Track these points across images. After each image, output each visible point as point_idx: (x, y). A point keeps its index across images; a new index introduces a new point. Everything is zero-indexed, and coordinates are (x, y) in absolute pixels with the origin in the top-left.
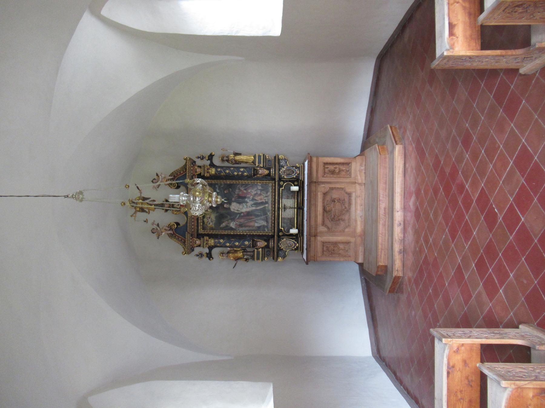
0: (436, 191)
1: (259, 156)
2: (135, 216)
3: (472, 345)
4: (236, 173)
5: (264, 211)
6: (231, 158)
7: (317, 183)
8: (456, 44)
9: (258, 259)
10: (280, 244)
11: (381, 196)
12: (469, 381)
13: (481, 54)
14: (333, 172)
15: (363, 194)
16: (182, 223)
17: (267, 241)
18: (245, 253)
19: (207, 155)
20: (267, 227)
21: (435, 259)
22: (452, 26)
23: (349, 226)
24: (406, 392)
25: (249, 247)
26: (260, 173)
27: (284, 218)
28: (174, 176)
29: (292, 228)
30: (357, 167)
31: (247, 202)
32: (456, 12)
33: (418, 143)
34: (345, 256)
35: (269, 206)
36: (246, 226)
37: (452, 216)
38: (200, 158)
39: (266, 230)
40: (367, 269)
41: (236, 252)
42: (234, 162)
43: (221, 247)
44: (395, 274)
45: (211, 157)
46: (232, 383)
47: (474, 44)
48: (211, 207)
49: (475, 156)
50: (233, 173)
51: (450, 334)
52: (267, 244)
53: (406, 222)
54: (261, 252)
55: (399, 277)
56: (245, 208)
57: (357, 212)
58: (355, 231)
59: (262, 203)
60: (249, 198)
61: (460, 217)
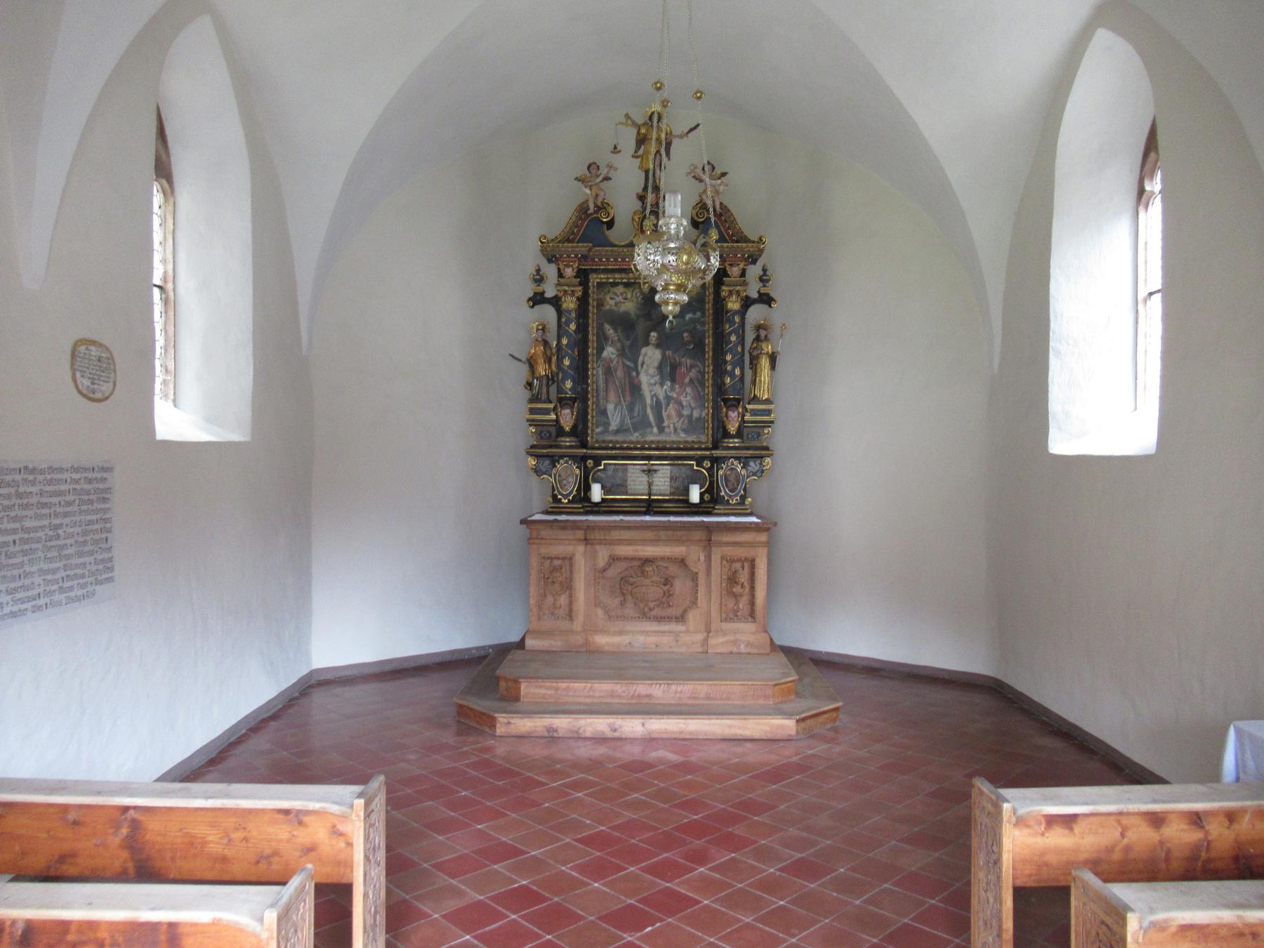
0: (690, 805)
1: (769, 412)
2: (627, 125)
3: (349, 864)
4: (729, 357)
5: (643, 424)
6: (764, 345)
7: (708, 544)
8: (1026, 831)
9: (532, 411)
11: (680, 688)
12: (268, 857)
13: (1004, 885)
14: (732, 580)
15: (683, 650)
16: (612, 235)
17: (574, 432)
18: (545, 382)
20: (606, 431)
21: (535, 804)
22: (1068, 821)
23: (610, 617)
24: (232, 739)
25: (560, 390)
26: (731, 413)
28: (721, 215)
29: (603, 488)
30: (745, 634)
31: (662, 385)
32: (1101, 830)
33: (800, 768)
34: (540, 608)
35: (653, 436)
36: (606, 382)
37: (633, 838)
39: (598, 430)
40: (509, 657)
41: (548, 360)
42: (755, 353)
43: (559, 326)
44: (501, 718)
45: (766, 299)
46: (249, 350)
47: (1027, 872)
48: (653, 291)
49: (770, 886)
50: (730, 351)
51: (373, 816)
52: (566, 431)
53: (620, 743)
55: (493, 726)
56: (648, 379)
57: (642, 636)
59: (660, 420)
60: (672, 389)
61: (634, 855)
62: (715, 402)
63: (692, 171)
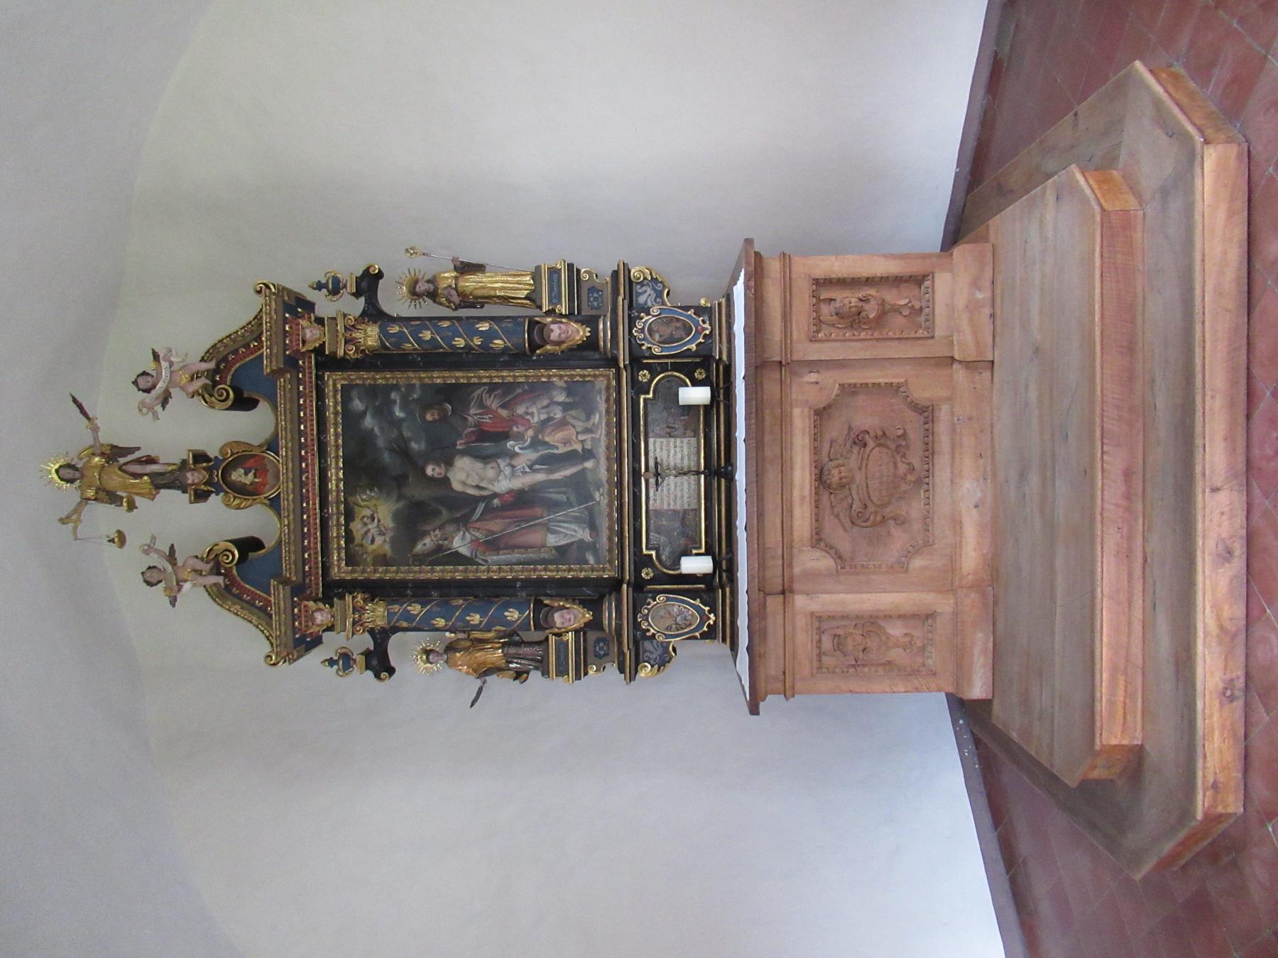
2: (79, 520)
4: (460, 342)
6: (443, 285)
10: (646, 618)
14: (854, 320)
17: (593, 604)
18: (512, 650)
19: (350, 270)
20: (593, 547)
23: (928, 544)
25: (525, 626)
27: (658, 513)
31: (514, 455)
35: (599, 468)
38: (324, 286)
39: (591, 560)
40: (1014, 735)
42: (456, 299)
45: (369, 282)
52: (601, 609)
54: (571, 647)
58: (953, 564)
59: (571, 457)
60: (519, 437)
62: (538, 365)
63: (151, 408)
